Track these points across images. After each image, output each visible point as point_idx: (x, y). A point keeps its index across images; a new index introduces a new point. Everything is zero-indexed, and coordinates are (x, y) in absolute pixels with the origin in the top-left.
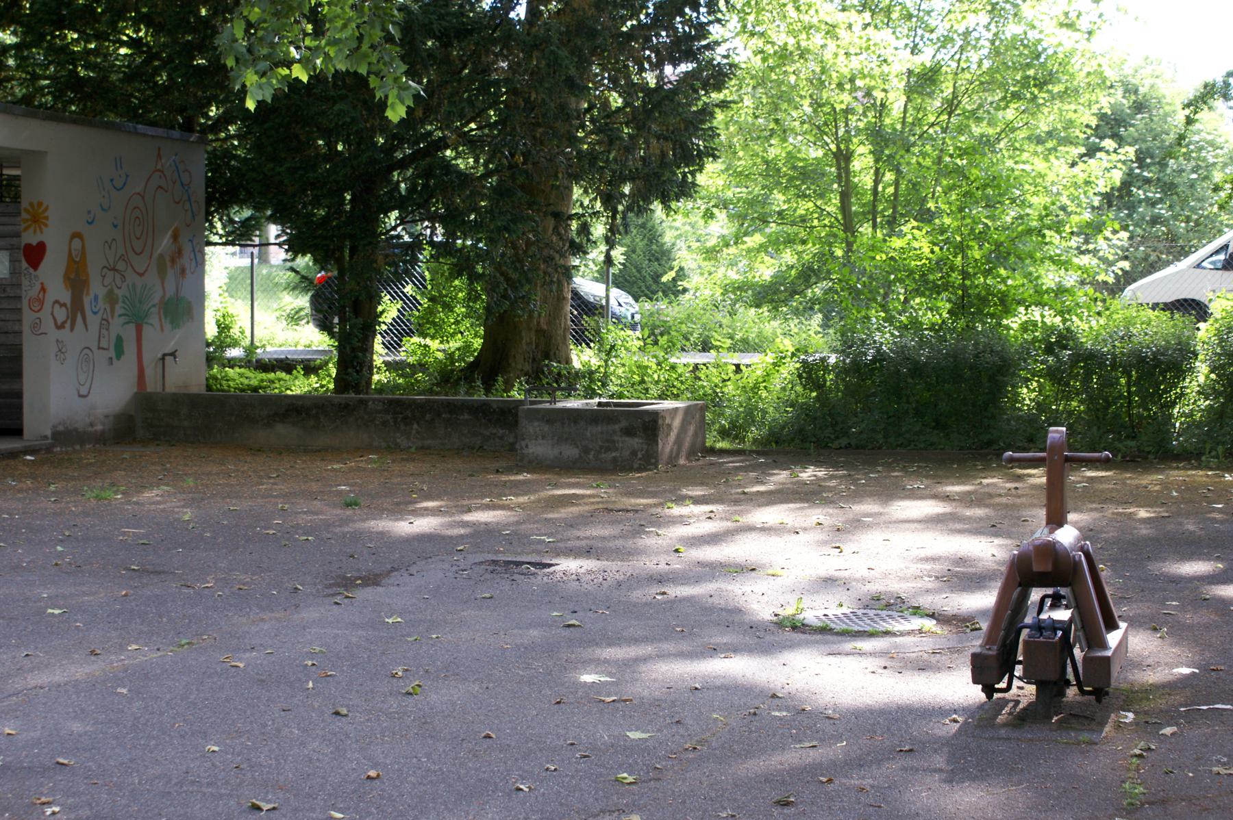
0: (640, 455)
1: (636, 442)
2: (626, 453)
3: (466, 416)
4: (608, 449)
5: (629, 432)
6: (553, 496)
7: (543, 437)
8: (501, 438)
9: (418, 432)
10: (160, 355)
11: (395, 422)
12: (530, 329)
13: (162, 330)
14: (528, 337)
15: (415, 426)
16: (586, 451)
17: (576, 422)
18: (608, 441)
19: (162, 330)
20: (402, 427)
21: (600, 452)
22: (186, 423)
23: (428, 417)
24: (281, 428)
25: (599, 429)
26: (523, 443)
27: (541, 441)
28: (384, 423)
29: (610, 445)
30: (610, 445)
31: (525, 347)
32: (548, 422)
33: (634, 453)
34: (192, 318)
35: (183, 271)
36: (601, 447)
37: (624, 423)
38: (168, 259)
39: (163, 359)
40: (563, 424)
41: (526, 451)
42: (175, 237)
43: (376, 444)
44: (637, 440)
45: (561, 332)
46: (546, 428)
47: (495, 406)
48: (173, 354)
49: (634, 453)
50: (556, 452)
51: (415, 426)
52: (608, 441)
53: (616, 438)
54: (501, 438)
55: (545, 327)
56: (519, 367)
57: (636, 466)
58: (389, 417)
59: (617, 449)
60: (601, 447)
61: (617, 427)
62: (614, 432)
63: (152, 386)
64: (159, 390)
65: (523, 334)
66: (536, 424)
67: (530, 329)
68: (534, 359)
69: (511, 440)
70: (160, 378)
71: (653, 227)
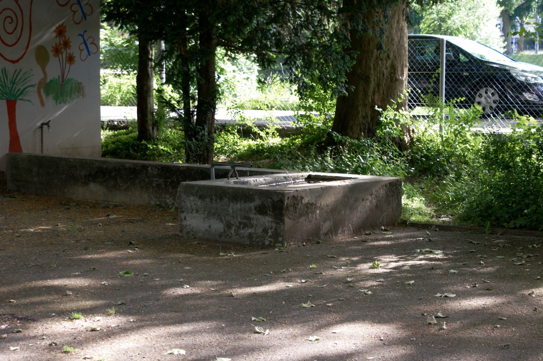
1: (267, 220)
2: (260, 230)
4: (245, 226)
5: (261, 210)
6: (374, 246)
10: (39, 124)
13: (43, 104)
16: (229, 226)
17: (221, 199)
19: (43, 104)
21: (239, 228)
22: (36, 179)
24: (93, 186)
26: (183, 216)
27: (195, 215)
28: (158, 186)
29: (246, 223)
30: (246, 223)
31: (361, 119)
33: (265, 231)
34: (83, 96)
35: (71, 59)
36: (240, 223)
37: (258, 202)
38: (50, 50)
39: (41, 127)
40: (211, 199)
42: (60, 32)
46: (199, 203)
48: (47, 124)
50: (206, 225)
53: (252, 216)
57: (267, 243)
58: (161, 181)
60: (240, 223)
61: (252, 205)
62: (250, 210)
63: (29, 146)
64: (38, 152)
65: (360, 109)
66: (192, 198)
70: (38, 140)
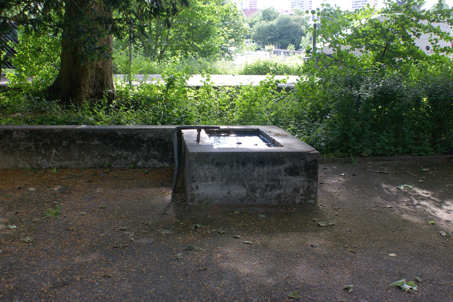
0: (301, 192)
2: (289, 191)
3: (96, 142)
4: (273, 188)
5: (293, 172)
7: (213, 179)
8: (126, 158)
9: (56, 155)
11: (37, 148)
12: (93, 68)
14: (91, 72)
15: (54, 151)
16: (253, 189)
18: (273, 180)
20: (43, 152)
21: (265, 190)
23: (64, 143)
25: (266, 169)
26: (194, 185)
27: (211, 183)
28: (28, 149)
31: (89, 79)
32: (217, 165)
33: (296, 190)
36: (267, 186)
37: (288, 164)
40: (232, 166)
41: (196, 192)
43: (21, 165)
44: (299, 178)
45: (109, 70)
46: (216, 170)
47: (120, 134)
49: (296, 190)
50: (225, 192)
51: (54, 151)
52: (273, 180)
53: (280, 178)
54: (126, 158)
55: (100, 67)
56: (87, 91)
58: (31, 144)
59: (281, 187)
60: (267, 186)
61: (282, 167)
62: (279, 172)
65: (89, 71)
66: (206, 167)
67: (93, 68)
68: (95, 86)
69: (134, 159)
71: (437, 7)
